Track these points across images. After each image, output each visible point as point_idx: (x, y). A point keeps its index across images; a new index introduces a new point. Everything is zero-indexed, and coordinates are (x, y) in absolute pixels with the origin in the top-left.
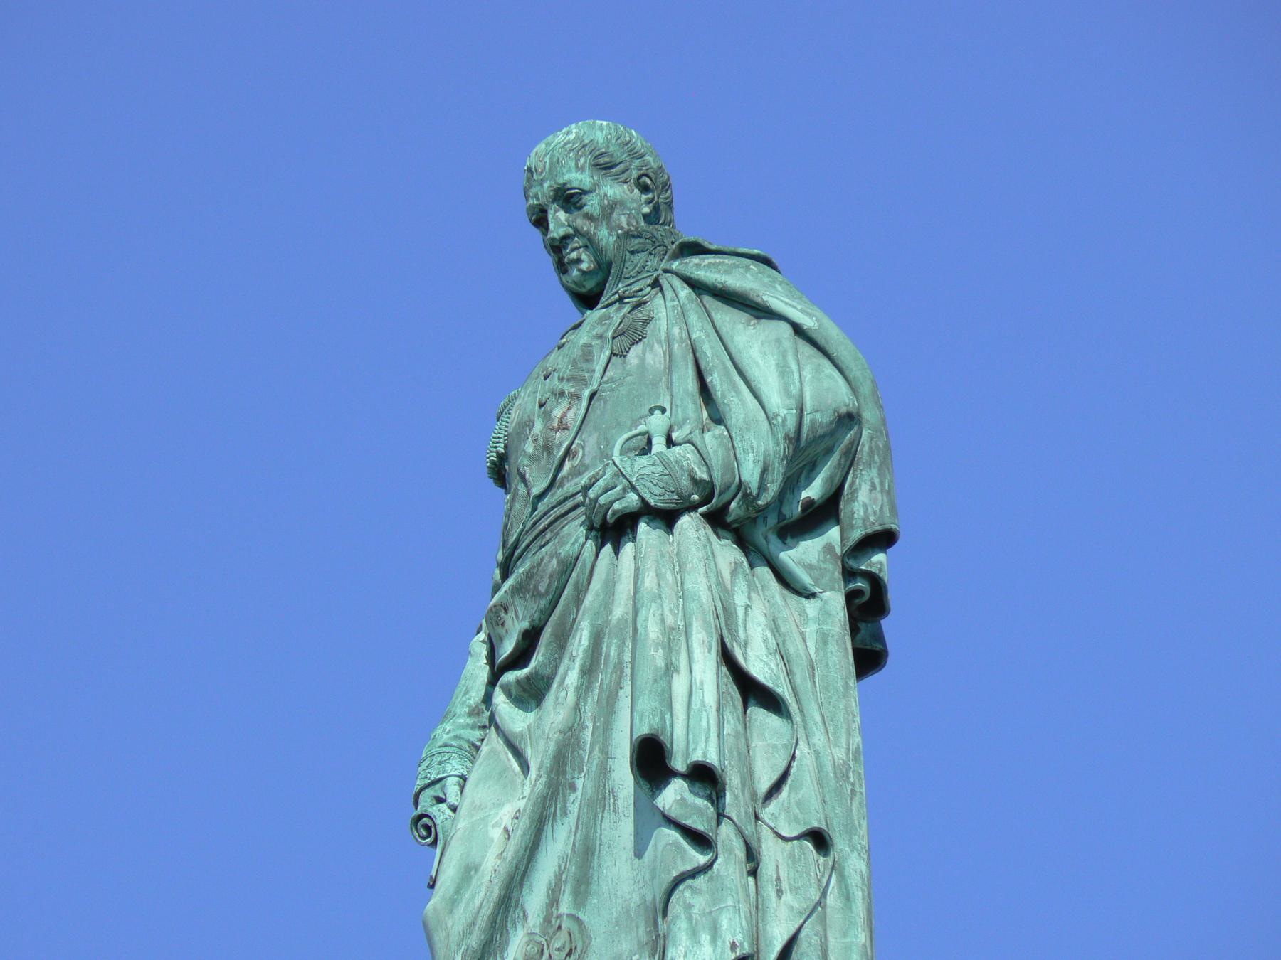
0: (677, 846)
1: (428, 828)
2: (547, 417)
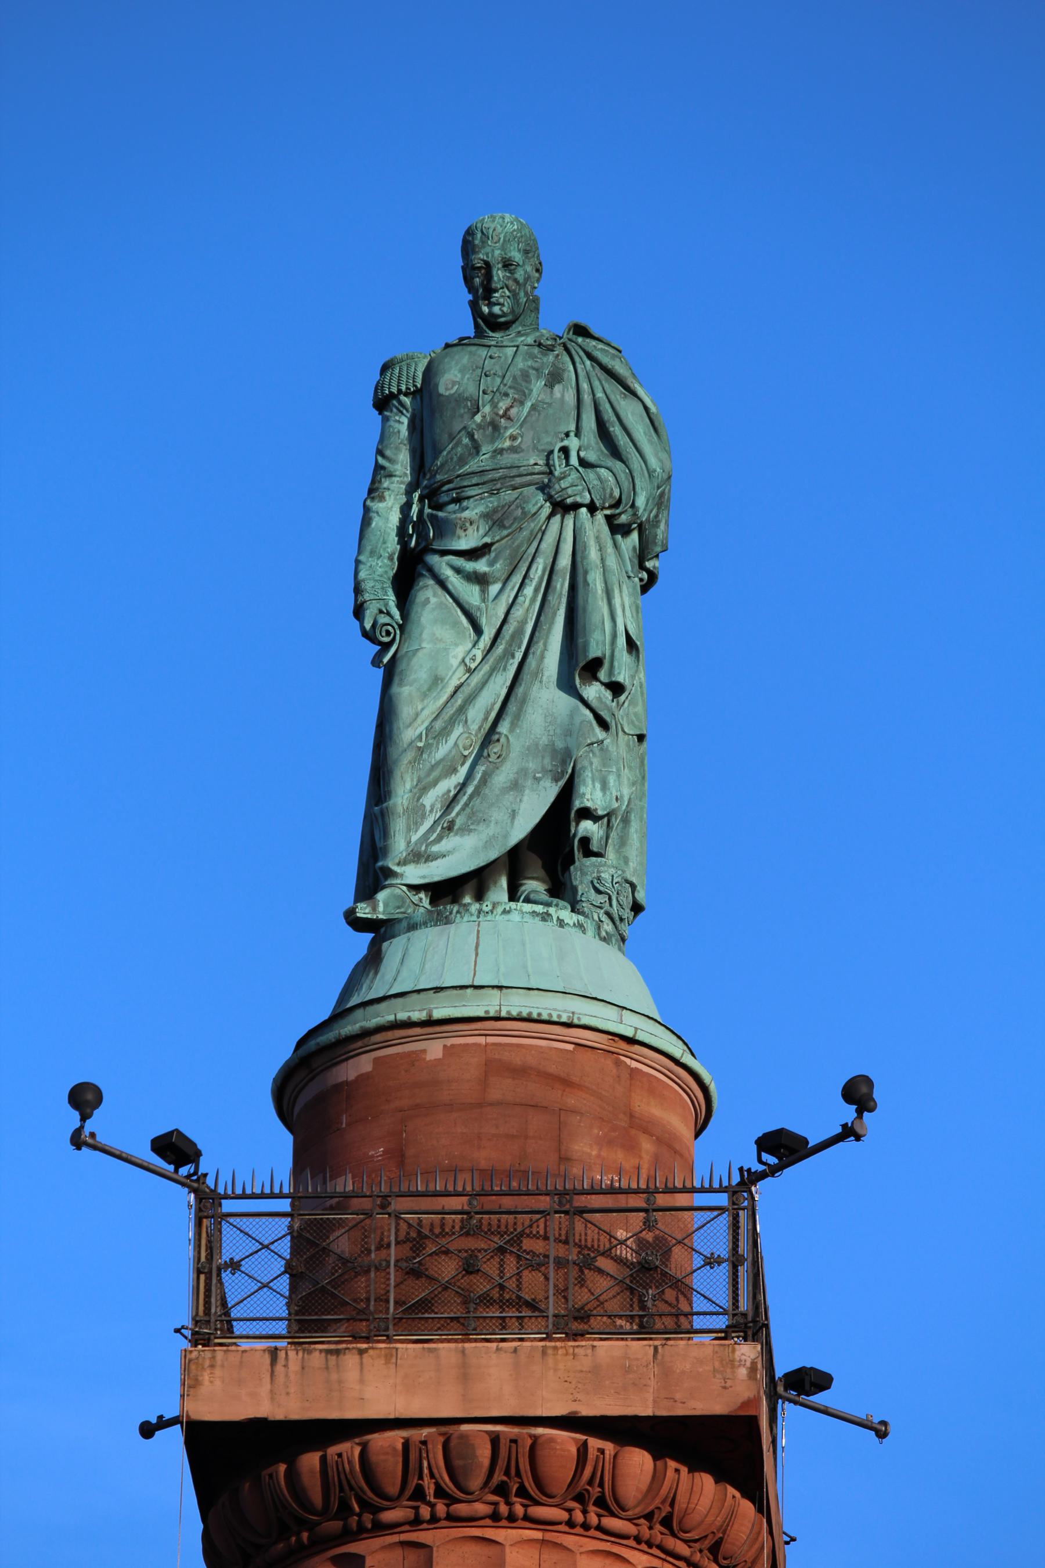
0: (590, 722)
2: (494, 406)
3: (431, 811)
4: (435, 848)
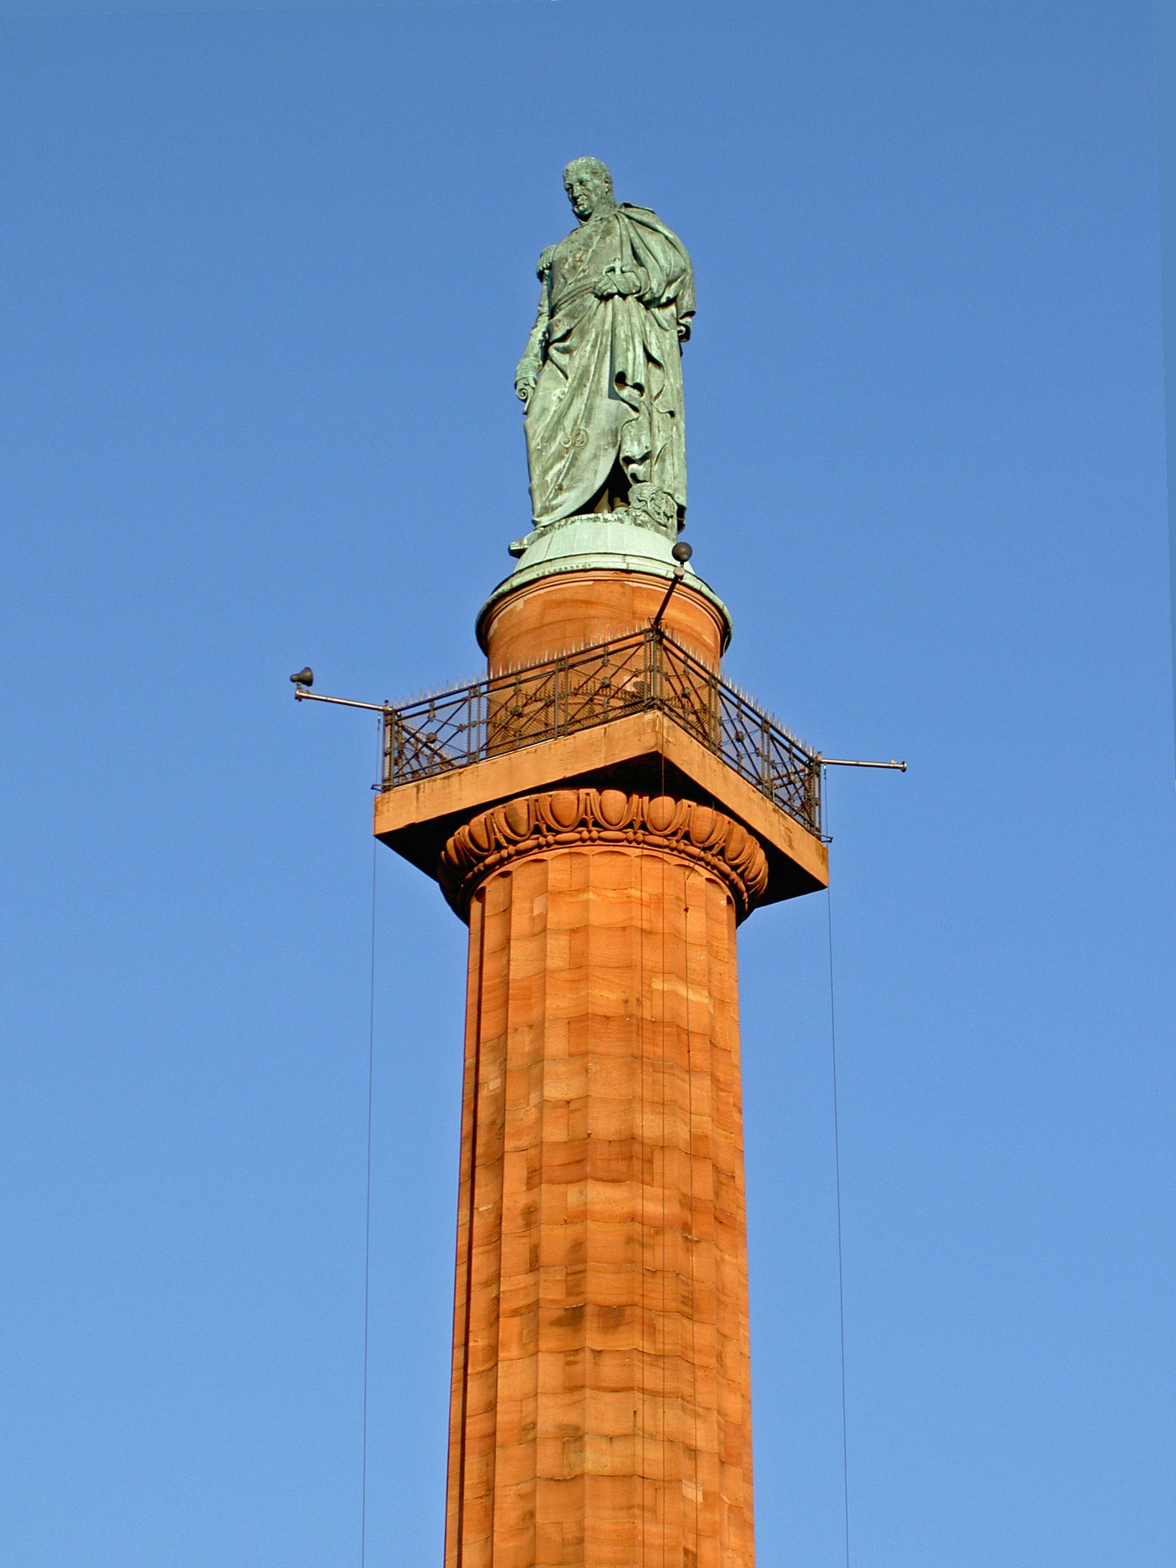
2: (574, 257)
4: (554, 502)
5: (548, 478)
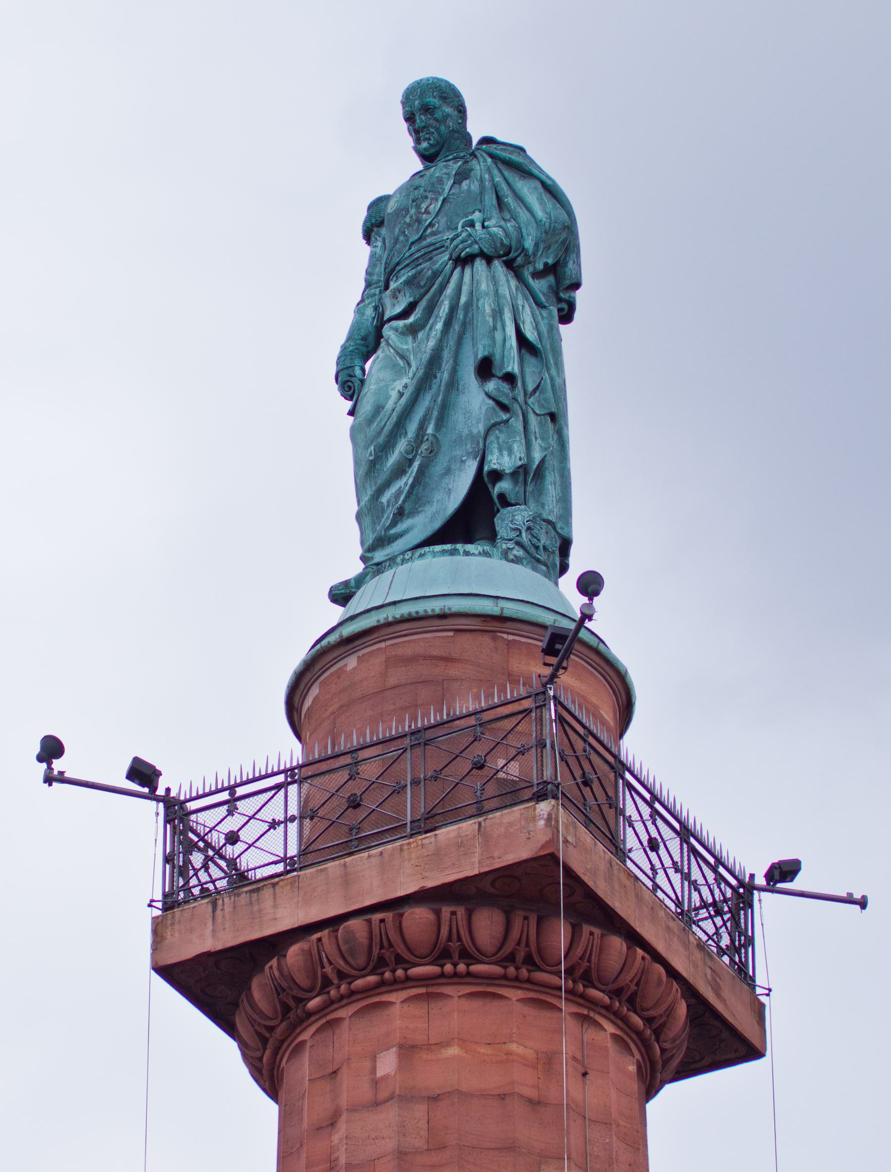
1: (350, 388)
2: (418, 207)
3: (388, 506)
4: (393, 531)
5: (384, 499)
